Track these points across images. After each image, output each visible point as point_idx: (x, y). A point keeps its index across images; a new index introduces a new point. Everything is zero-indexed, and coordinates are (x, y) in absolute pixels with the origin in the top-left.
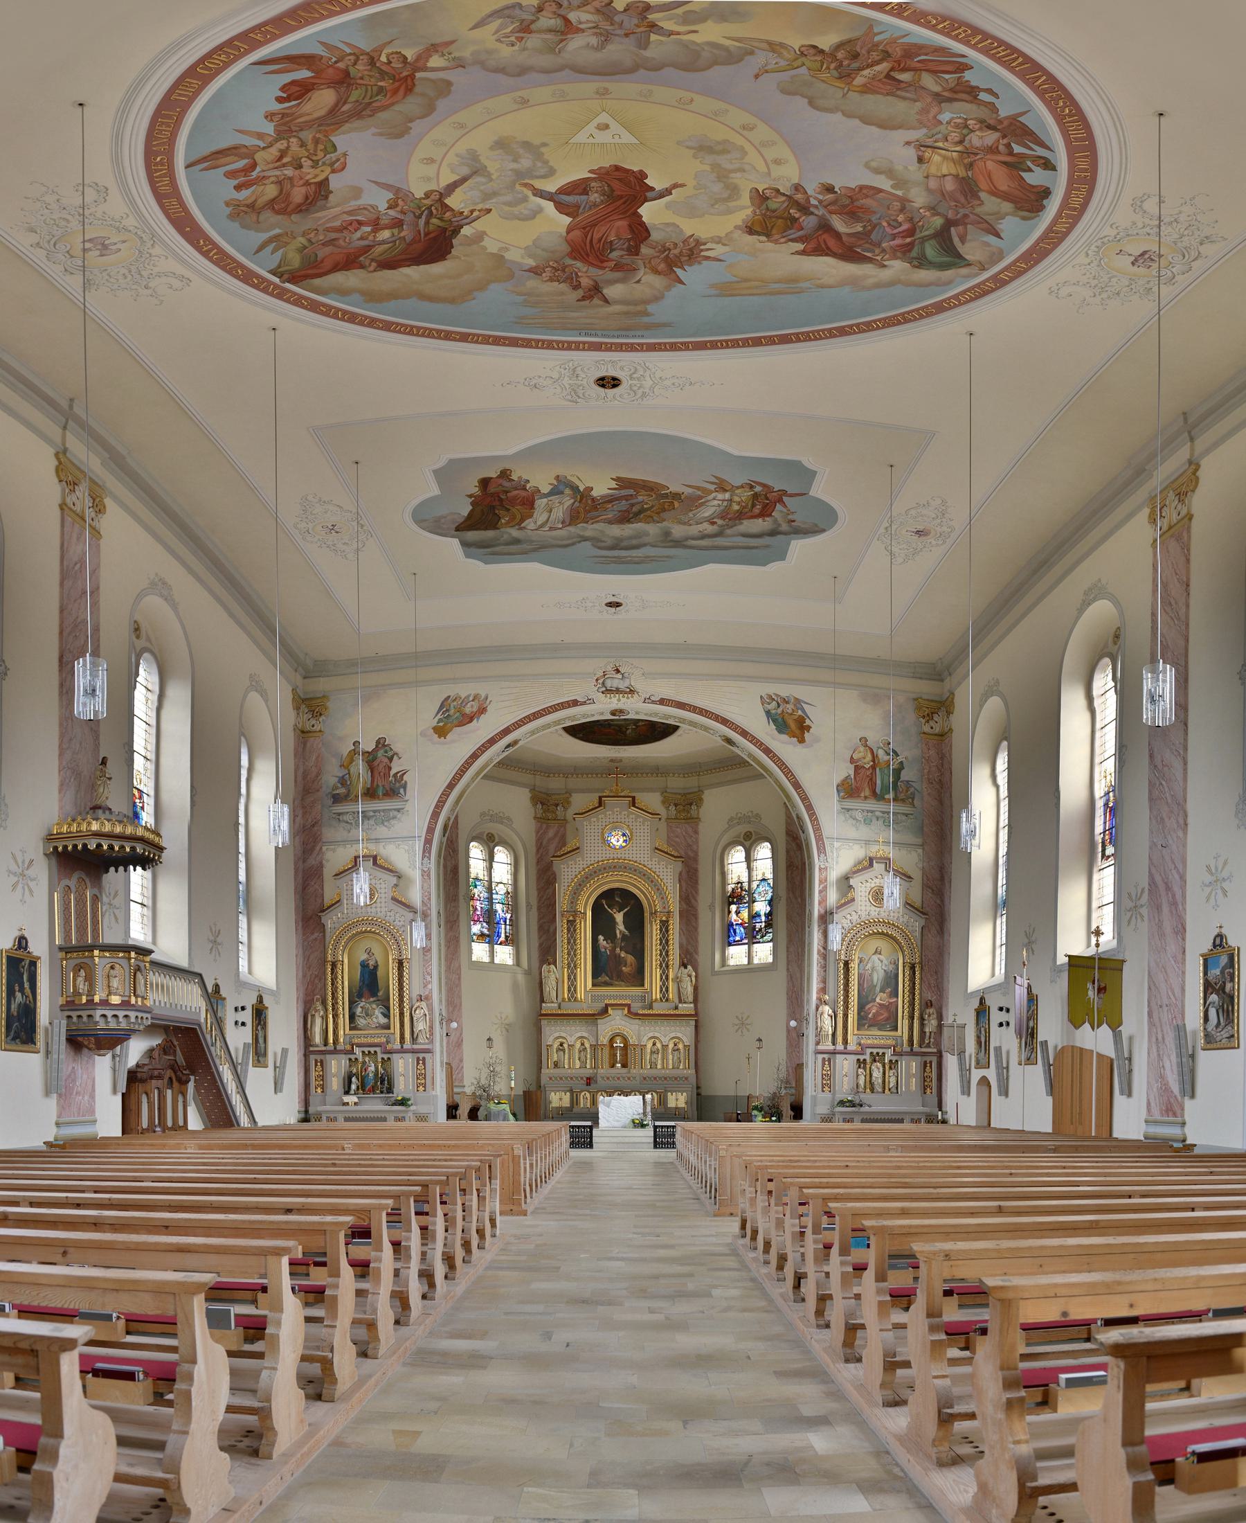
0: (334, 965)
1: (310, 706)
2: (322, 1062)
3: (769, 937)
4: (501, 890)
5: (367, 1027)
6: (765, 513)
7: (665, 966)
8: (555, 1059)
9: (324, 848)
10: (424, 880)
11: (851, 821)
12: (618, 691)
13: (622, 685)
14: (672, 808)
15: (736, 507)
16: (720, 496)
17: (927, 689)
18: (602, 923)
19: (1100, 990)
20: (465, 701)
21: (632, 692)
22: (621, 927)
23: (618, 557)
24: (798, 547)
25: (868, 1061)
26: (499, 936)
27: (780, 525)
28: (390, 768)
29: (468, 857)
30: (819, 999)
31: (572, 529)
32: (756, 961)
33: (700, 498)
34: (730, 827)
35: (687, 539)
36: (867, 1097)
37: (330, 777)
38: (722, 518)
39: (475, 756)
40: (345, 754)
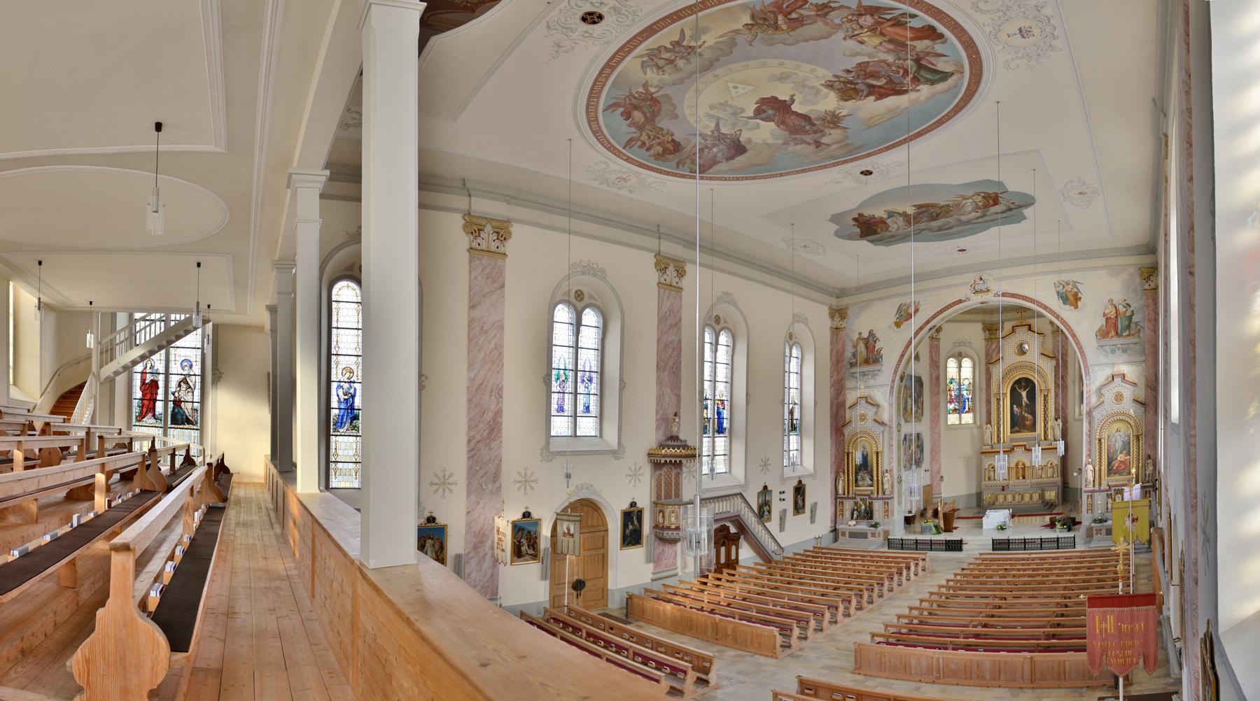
1: (839, 313)
4: (966, 382)
6: (996, 203)
12: (981, 291)
18: (1015, 398)
22: (1025, 399)
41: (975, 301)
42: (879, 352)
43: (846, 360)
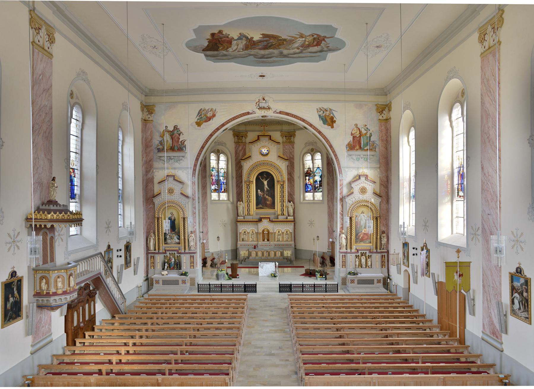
0: (158, 219)
1: (148, 109)
2: (153, 257)
3: (321, 190)
4: (222, 171)
6: (318, 44)
7: (282, 201)
11: (352, 160)
12: (264, 108)
13: (266, 106)
14: (284, 138)
15: (307, 43)
16: (301, 39)
18: (259, 185)
19: (460, 276)
20: (207, 112)
21: (269, 108)
22: (266, 186)
26: (222, 189)
29: (210, 159)
30: (340, 231)
31: (246, 52)
32: (316, 199)
33: (294, 40)
34: (306, 146)
35: (289, 54)
36: (359, 270)
37: (156, 140)
38: (302, 47)
39: (211, 135)
40: (162, 131)
41: (259, 114)
42: (183, 142)
43: (154, 146)
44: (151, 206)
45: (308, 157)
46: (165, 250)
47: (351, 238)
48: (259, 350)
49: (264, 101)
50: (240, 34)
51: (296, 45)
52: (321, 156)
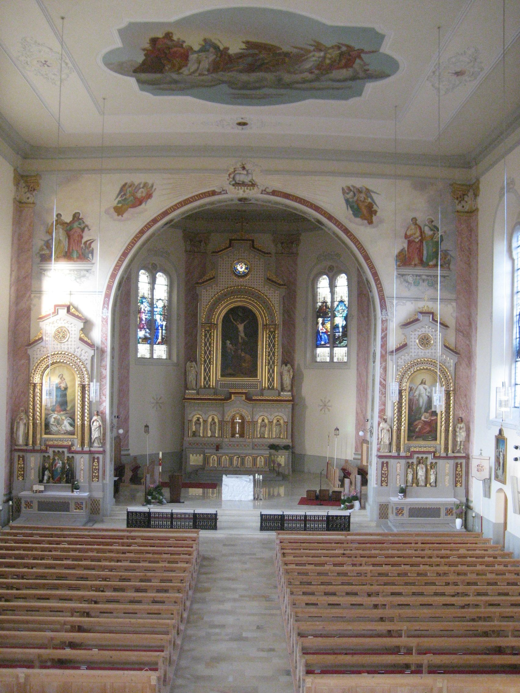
2: (23, 457)
4: (160, 304)
5: (58, 433)
8: (194, 430)
9: (32, 295)
10: (103, 326)
12: (243, 184)
13: (247, 179)
14: (279, 245)
15: (328, 61)
16: (317, 54)
17: (459, 175)
18: (229, 333)
20: (138, 187)
22: (242, 334)
23: (245, 93)
24: (370, 87)
25: (415, 463)
26: (157, 338)
27: (358, 73)
28: (82, 237)
29: (137, 281)
31: (214, 75)
33: (303, 55)
44: (23, 361)
45: (323, 283)
46: (47, 446)
47: (399, 430)
48: (217, 630)
49: (245, 172)
50: (205, 40)
51: (308, 65)
52: (348, 280)
